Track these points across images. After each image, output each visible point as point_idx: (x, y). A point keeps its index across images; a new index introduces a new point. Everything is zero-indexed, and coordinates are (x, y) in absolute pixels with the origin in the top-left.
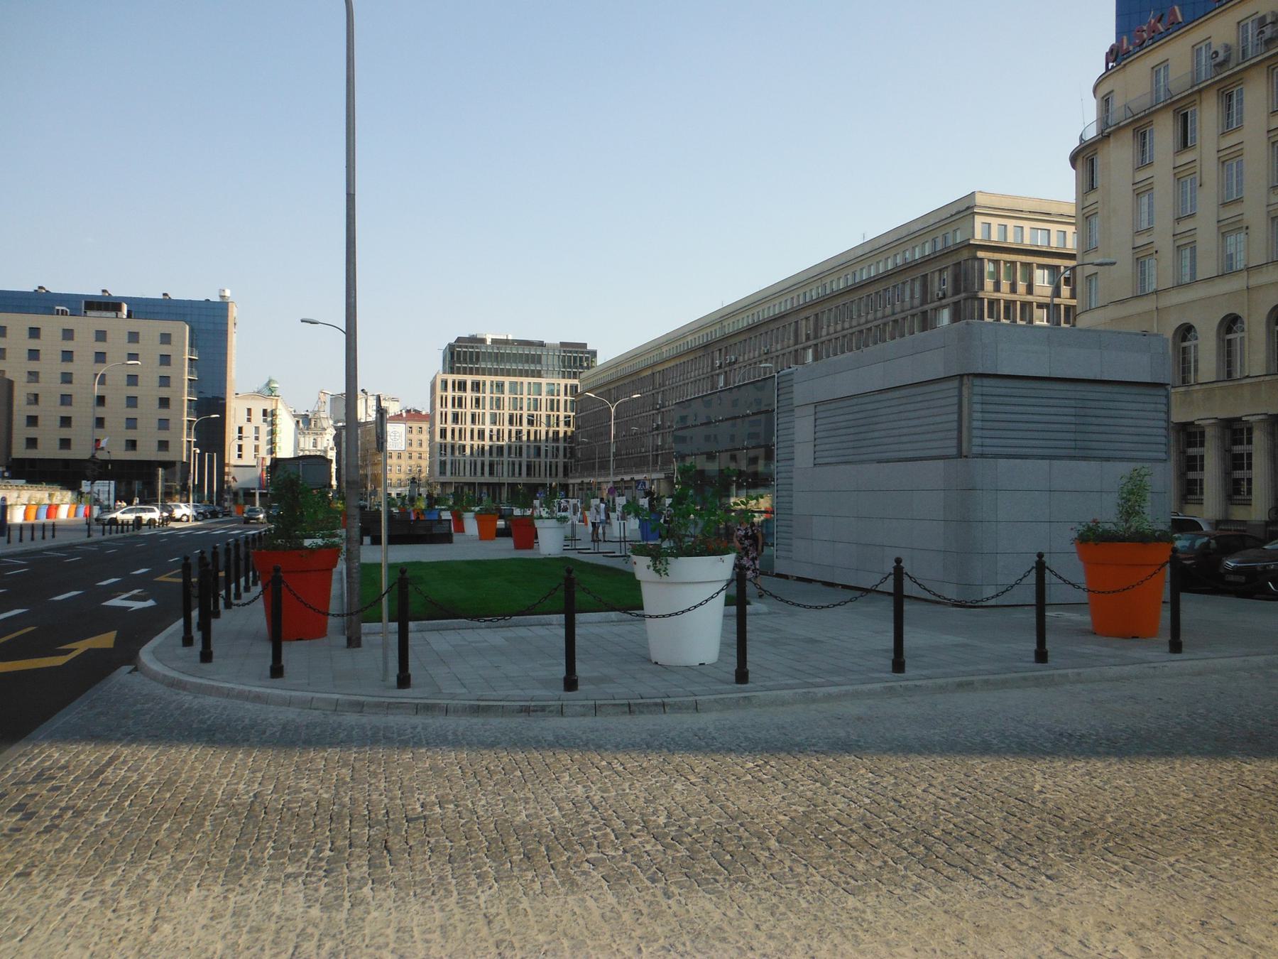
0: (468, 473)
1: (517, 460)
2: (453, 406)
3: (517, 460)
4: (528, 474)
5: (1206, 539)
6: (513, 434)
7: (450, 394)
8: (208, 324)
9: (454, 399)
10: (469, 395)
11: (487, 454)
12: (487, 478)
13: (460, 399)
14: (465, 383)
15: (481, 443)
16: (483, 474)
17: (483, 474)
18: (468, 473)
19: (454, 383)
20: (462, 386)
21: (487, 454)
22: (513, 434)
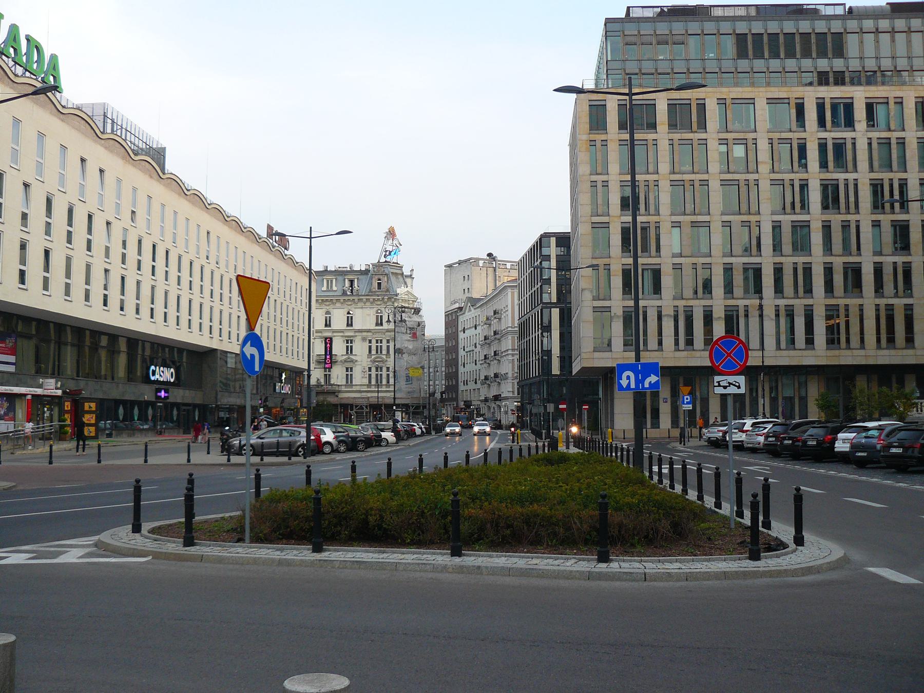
0: (668, 341)
1: (799, 304)
2: (824, 165)
3: (799, 304)
4: (832, 341)
5: (843, 442)
6: (786, 231)
7: (812, 134)
8: (608, 21)
9: (823, 147)
10: (861, 134)
11: (718, 289)
12: (820, 354)
13: (839, 148)
14: (849, 107)
15: (801, 260)
16: (810, 341)
17: (810, 341)
18: (668, 341)
19: (821, 107)
20: (843, 113)
21: (718, 289)
22: (786, 231)
